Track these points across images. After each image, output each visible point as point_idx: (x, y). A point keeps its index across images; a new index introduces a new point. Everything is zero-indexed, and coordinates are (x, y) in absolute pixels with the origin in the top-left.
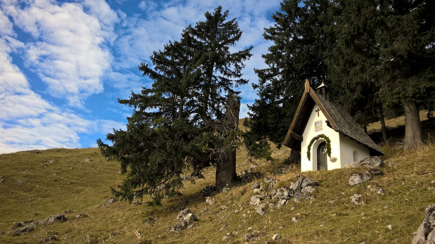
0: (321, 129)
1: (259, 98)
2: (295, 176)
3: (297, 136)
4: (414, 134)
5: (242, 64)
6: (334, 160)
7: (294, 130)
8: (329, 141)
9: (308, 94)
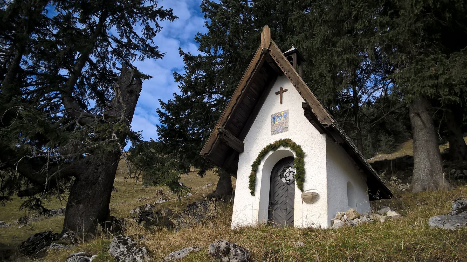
0: (285, 129)
1: (180, 94)
2: (211, 250)
3: (232, 140)
4: (431, 165)
5: (157, 25)
6: (312, 199)
7: (228, 125)
8: (301, 154)
9: (266, 53)
